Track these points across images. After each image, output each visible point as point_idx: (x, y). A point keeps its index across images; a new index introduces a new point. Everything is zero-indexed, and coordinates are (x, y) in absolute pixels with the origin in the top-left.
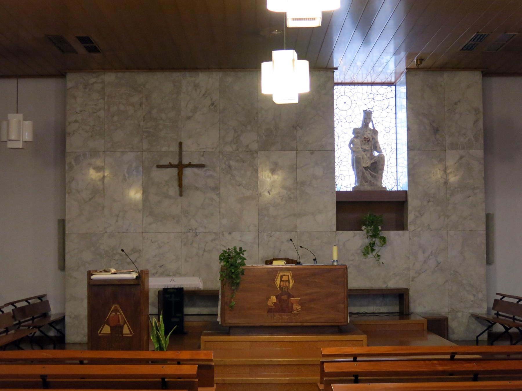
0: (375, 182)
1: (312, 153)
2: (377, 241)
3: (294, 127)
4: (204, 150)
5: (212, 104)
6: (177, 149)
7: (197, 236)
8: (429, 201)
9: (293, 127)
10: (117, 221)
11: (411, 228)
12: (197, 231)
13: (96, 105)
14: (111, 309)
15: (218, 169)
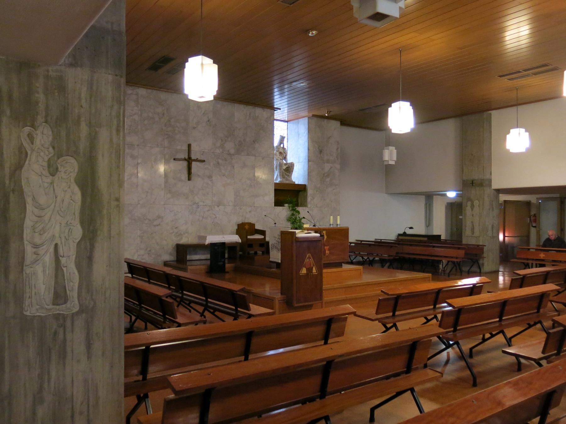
0: (289, 178)
1: (263, 159)
2: (295, 213)
3: (254, 142)
4: (203, 151)
5: (209, 121)
6: (187, 148)
7: (199, 208)
8: (317, 191)
9: (253, 141)
10: (147, 196)
11: (309, 206)
12: (199, 204)
13: (132, 110)
14: (306, 257)
15: (212, 164)
